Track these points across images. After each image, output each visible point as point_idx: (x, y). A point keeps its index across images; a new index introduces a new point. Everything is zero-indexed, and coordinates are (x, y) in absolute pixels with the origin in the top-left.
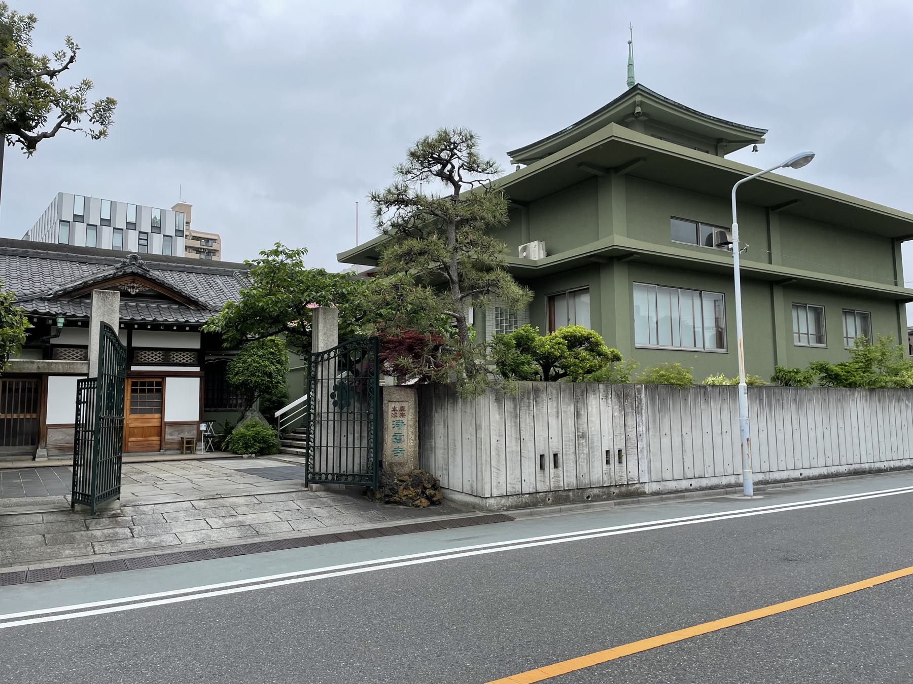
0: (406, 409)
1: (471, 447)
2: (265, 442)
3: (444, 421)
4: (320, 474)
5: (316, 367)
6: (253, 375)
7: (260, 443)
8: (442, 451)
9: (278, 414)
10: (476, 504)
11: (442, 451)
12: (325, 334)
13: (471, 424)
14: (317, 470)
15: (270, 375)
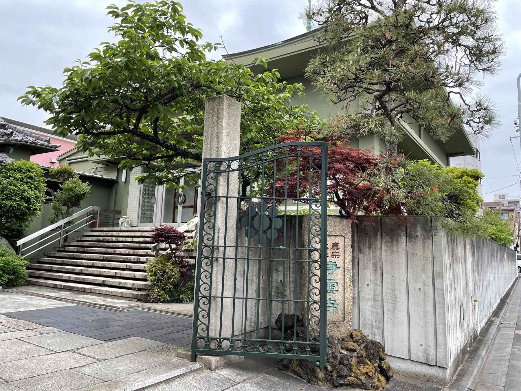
0: (341, 246)
1: (425, 301)
2: (14, 273)
3: (375, 265)
4: (220, 340)
5: (216, 179)
6: (8, 198)
7: (8, 274)
8: (370, 303)
9: (20, 242)
10: (437, 377)
11: (370, 303)
12: (228, 134)
13: (424, 270)
14: (212, 334)
15: (28, 200)
